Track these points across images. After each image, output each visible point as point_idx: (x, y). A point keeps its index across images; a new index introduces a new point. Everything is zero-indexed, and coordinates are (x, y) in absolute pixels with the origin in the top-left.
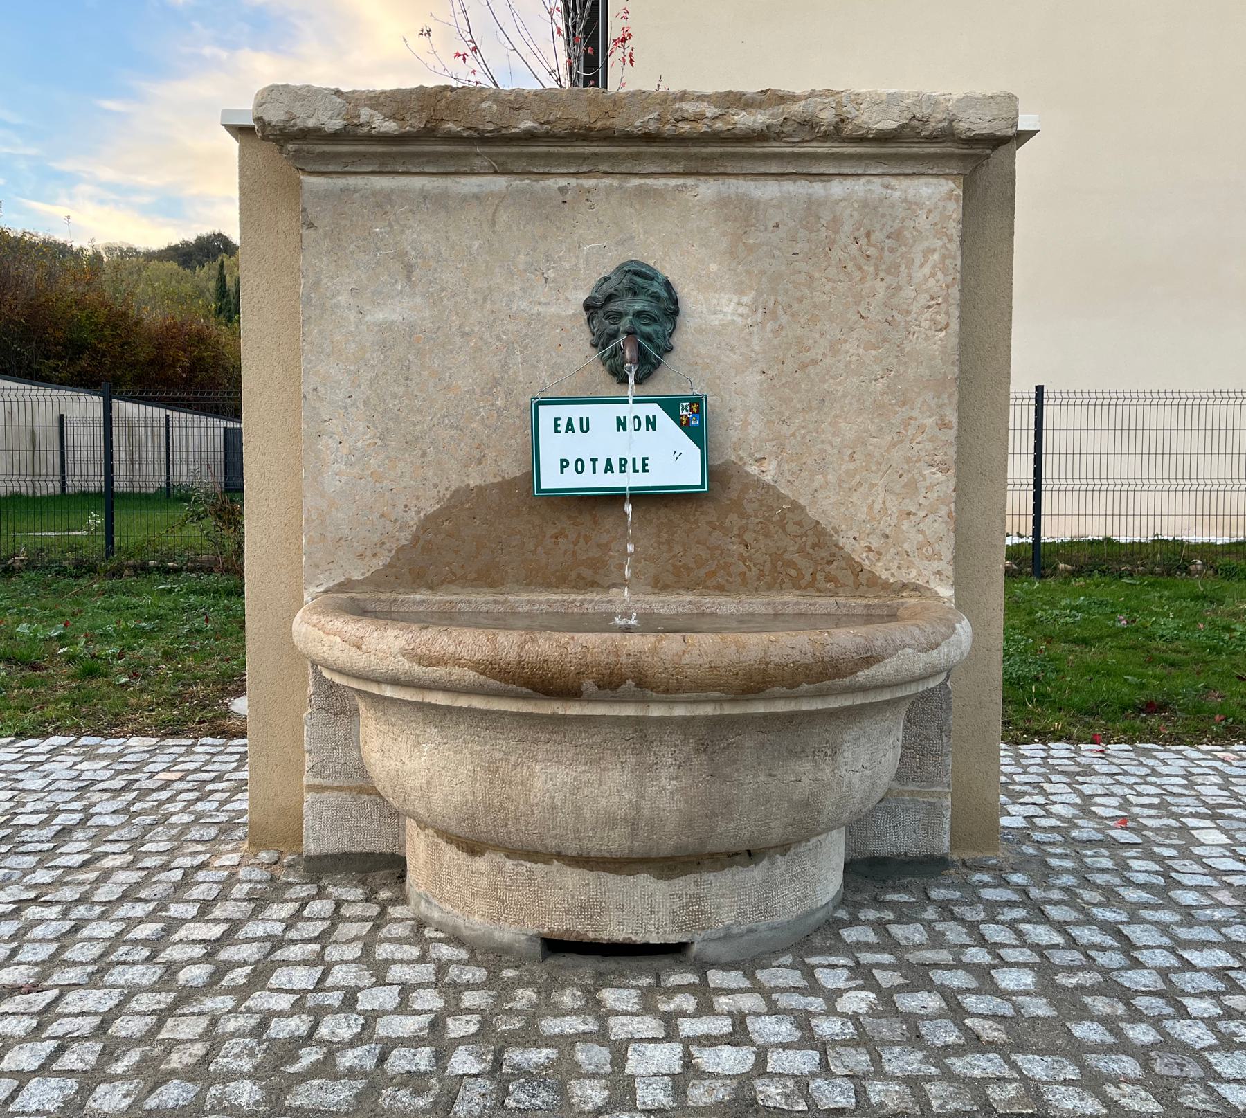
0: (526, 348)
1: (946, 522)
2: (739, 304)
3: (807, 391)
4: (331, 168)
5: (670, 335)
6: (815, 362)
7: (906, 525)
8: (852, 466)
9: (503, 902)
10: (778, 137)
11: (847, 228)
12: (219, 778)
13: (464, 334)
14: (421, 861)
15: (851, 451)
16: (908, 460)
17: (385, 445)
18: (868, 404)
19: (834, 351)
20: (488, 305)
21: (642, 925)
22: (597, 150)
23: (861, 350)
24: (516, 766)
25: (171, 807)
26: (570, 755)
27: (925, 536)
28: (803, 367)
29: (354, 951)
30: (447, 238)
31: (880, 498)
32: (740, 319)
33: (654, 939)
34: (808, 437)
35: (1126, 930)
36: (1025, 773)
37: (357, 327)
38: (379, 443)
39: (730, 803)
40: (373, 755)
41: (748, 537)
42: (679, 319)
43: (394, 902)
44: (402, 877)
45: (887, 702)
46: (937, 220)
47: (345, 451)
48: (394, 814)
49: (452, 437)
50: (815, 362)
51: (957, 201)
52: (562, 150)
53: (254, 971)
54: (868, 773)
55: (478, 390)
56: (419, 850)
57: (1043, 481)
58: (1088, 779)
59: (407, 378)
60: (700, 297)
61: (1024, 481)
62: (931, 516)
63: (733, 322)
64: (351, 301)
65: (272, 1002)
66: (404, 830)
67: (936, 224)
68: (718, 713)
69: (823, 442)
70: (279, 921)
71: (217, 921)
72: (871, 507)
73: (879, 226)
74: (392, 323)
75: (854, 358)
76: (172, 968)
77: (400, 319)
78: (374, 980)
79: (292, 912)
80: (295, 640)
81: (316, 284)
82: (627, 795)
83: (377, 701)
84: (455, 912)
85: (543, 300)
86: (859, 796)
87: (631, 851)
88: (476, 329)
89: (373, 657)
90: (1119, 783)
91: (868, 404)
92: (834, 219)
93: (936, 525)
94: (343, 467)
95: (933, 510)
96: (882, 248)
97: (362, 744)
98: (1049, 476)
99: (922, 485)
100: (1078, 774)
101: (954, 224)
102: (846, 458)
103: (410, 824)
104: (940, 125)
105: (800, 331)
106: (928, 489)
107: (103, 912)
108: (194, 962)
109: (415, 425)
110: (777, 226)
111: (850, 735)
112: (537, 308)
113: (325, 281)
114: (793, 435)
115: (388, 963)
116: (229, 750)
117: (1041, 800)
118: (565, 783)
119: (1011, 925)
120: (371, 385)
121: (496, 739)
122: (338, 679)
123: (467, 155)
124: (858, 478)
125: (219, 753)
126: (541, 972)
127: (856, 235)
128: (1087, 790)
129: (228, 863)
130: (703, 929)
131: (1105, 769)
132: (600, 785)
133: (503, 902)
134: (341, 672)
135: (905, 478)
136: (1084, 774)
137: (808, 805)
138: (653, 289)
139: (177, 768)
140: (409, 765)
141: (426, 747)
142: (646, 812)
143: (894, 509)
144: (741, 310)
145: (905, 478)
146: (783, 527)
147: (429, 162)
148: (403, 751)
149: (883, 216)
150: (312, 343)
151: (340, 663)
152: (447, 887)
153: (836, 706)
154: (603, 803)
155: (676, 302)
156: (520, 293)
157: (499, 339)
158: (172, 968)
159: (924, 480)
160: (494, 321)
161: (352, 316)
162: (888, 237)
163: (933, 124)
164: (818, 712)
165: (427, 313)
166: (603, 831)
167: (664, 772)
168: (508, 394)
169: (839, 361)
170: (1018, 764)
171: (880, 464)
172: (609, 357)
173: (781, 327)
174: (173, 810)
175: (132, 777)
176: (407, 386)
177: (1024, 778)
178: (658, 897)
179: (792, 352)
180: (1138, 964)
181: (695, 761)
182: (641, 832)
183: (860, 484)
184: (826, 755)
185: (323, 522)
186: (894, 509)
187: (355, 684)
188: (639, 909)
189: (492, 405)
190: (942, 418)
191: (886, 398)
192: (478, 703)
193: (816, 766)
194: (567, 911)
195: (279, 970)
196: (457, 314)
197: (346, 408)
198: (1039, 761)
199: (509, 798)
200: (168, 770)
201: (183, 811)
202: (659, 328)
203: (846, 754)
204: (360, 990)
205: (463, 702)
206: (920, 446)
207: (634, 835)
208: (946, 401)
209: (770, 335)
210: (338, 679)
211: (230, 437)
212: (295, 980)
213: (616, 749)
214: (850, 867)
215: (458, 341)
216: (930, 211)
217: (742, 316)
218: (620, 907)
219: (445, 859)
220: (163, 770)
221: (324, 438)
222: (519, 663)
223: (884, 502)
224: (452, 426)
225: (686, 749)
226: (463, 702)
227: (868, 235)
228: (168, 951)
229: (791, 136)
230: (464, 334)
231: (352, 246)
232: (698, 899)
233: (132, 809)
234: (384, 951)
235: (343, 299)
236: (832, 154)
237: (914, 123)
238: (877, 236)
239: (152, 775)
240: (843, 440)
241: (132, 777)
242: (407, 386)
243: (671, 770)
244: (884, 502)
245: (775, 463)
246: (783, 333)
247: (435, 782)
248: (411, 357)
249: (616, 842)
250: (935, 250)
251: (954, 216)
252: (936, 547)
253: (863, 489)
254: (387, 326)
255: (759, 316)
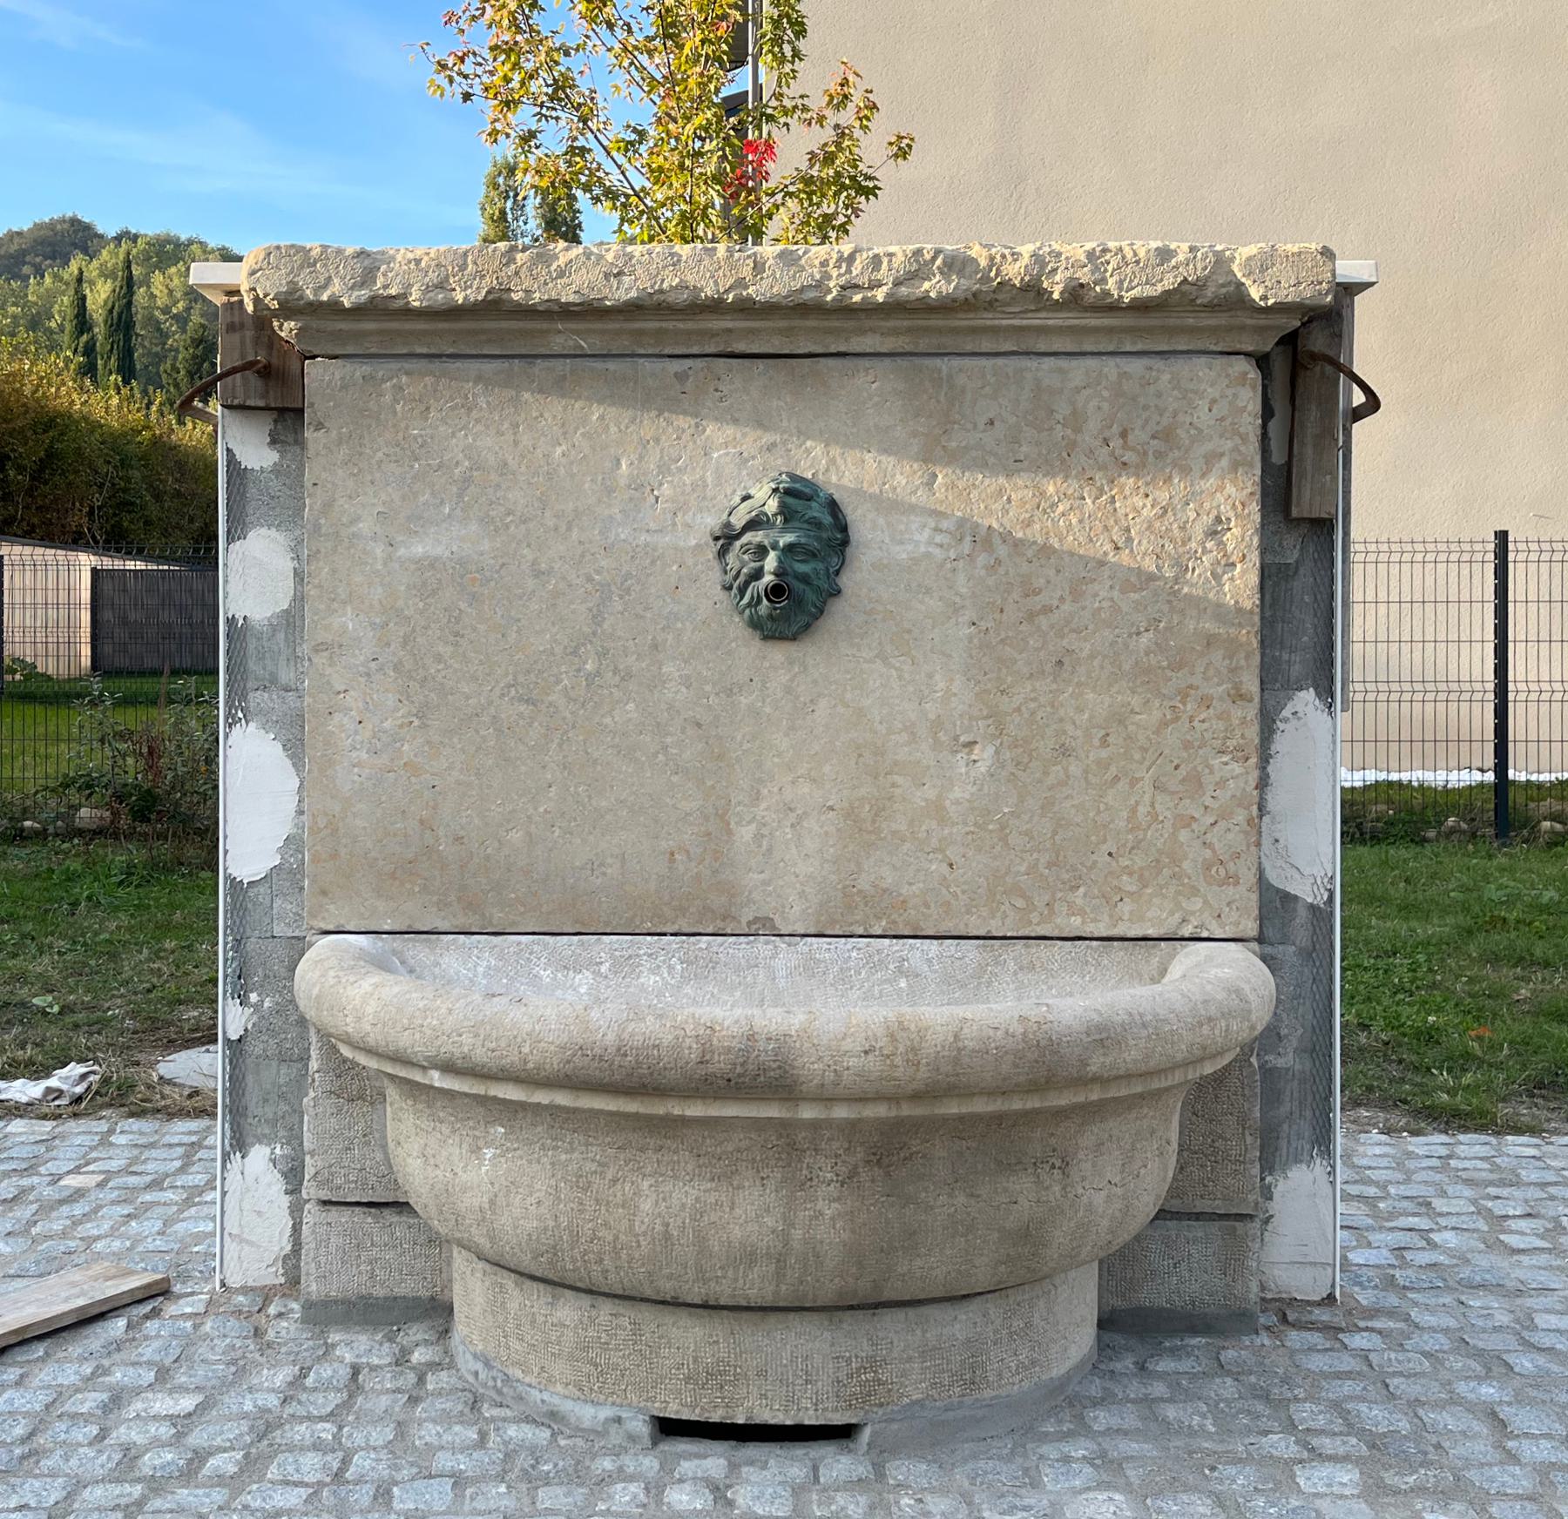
0: (628, 591)
1: (1246, 833)
2: (937, 530)
3: (1036, 649)
4: (350, 350)
5: (837, 573)
6: (1047, 610)
7: (1184, 836)
8: (1104, 754)
9: (596, 1365)
10: (991, 305)
11: (1093, 425)
12: (156, 1184)
13: (538, 574)
14: (478, 1309)
15: (1103, 732)
16: (1187, 745)
17: (424, 726)
18: (1126, 667)
19: (1076, 595)
20: (575, 533)
21: (791, 1399)
22: (730, 325)
23: (1116, 594)
24: (615, 1181)
25: (90, 1229)
26: (690, 1167)
27: (1214, 851)
28: (1031, 616)
29: (381, 1434)
30: (516, 443)
31: (1147, 798)
32: (937, 551)
33: (809, 1419)
34: (1040, 714)
35: (1505, 1412)
36: (1408, 1181)
37: (385, 564)
38: (416, 723)
39: (915, 1232)
40: (410, 1160)
41: (952, 853)
42: (849, 551)
43: (434, 1366)
44: (445, 1333)
45: (1141, 1096)
46: (1225, 412)
47: (368, 734)
48: (435, 1241)
49: (520, 715)
50: (1047, 610)
51: (1254, 388)
52: (681, 325)
53: (246, 1456)
54: (1119, 1191)
55: (558, 650)
56: (471, 1290)
57: (1511, 686)
58: (1505, 1192)
59: (457, 634)
60: (881, 521)
61: (1478, 686)
62: (1222, 824)
63: (928, 555)
64: (377, 529)
65: (277, 1497)
66: (449, 1264)
67: (1222, 419)
68: (893, 1113)
69: (1061, 720)
70: (274, 1390)
71: (183, 1389)
72: (1134, 811)
73: (1140, 422)
74: (437, 559)
75: (1106, 604)
76: (131, 1456)
77: (447, 553)
78: (415, 1470)
79: (290, 1379)
80: (302, 1004)
81: (328, 506)
82: (769, 1221)
83: (414, 1089)
84: (527, 1380)
85: (652, 526)
86: (1105, 1223)
87: (776, 1293)
88: (556, 566)
89: (417, 1036)
90: (1552, 1198)
91: (1126, 667)
92: (1074, 412)
93: (1230, 836)
94: (365, 756)
95: (1225, 815)
96: (1145, 453)
97: (391, 1145)
98: (1521, 677)
99: (1209, 780)
100: (1491, 1183)
101: (1250, 419)
102: (1096, 742)
103: (459, 1258)
104: (1224, 290)
105: (1025, 568)
106: (1221, 784)
107: (22, 1376)
108: (157, 1444)
109: (468, 698)
110: (992, 423)
111: (1088, 1139)
112: (643, 537)
113: (341, 501)
114: (1018, 710)
115: (431, 1450)
116: (168, 1139)
117: (1423, 1223)
118: (684, 1205)
119: (1337, 1406)
120: (405, 643)
121: (587, 1145)
122: (362, 1059)
123: (544, 332)
124: (1113, 770)
125: (152, 1145)
126: (649, 1464)
127: (1107, 434)
128: (1498, 1208)
129: (188, 1310)
130: (881, 1405)
131: (1534, 1176)
132: (732, 1208)
133: (596, 1365)
134: (370, 1052)
135: (1183, 771)
136: (1502, 1183)
137: (1029, 1236)
138: (811, 514)
139: (91, 1168)
140: (464, 1177)
141: (489, 1153)
142: (795, 1245)
143: (1168, 814)
144: (938, 539)
145: (1183, 771)
146: (1004, 840)
147: (489, 341)
148: (456, 1159)
149: (1146, 407)
150: (320, 586)
151: (371, 1041)
152: (515, 1345)
153: (1063, 1103)
154: (737, 1232)
155: (844, 529)
156: (619, 517)
157: (590, 579)
158: (131, 1456)
159: (1212, 773)
160: (583, 556)
161: (379, 550)
162: (1153, 437)
163: (1210, 292)
164: (1036, 1112)
165: (486, 545)
166: (736, 1269)
167: (823, 1191)
168: (602, 654)
169: (1083, 608)
170: (1400, 1166)
171: (1146, 750)
172: (749, 605)
173: (998, 562)
174: (95, 1232)
175: (25, 1182)
176: (456, 644)
177: (1404, 1190)
178: (818, 1359)
179: (1015, 596)
180: (1513, 1458)
181: (864, 1176)
182: (789, 1272)
183: (1116, 778)
184: (1053, 1166)
185: (335, 831)
186: (1168, 814)
187: (389, 1068)
188: (788, 1372)
189: (579, 670)
190: (1237, 687)
191: (1153, 660)
192: (562, 1099)
193: (1038, 1182)
194: (688, 1379)
195: (281, 1457)
196: (529, 546)
197: (368, 675)
198: (1435, 1162)
199: (606, 1224)
200: (77, 1170)
201: (112, 1233)
202: (820, 566)
203: (1083, 1165)
204: (396, 1483)
205: (542, 1097)
206: (1206, 725)
207: (779, 1275)
208: (1243, 662)
209: (983, 572)
210: (362, 1059)
211: (107, 587)
212: (305, 1469)
213: (754, 1160)
214: (1106, 1323)
215: (531, 583)
216: (1214, 401)
217: (941, 546)
218: (762, 1373)
219: (513, 1306)
220: (69, 1173)
221: (337, 717)
222: (619, 1049)
223: (1152, 805)
224: (521, 699)
225: (852, 1160)
226: (542, 1097)
227: (1124, 434)
228: (122, 1430)
229: (1009, 305)
230: (538, 574)
231: (380, 454)
232: (872, 1364)
233: (34, 1231)
234: (428, 1433)
235: (364, 527)
236: (1069, 327)
237: (1186, 287)
238: (1138, 436)
239: (56, 1179)
240: (1091, 717)
241: (25, 1182)
242: (456, 644)
243: (832, 1188)
244: (1152, 805)
245: (991, 750)
246: (1001, 571)
247: (501, 1200)
248: (463, 605)
249: (755, 1285)
250: (1222, 455)
251: (1250, 408)
252: (1231, 866)
253: (1122, 785)
254: (433, 563)
255: (967, 546)
